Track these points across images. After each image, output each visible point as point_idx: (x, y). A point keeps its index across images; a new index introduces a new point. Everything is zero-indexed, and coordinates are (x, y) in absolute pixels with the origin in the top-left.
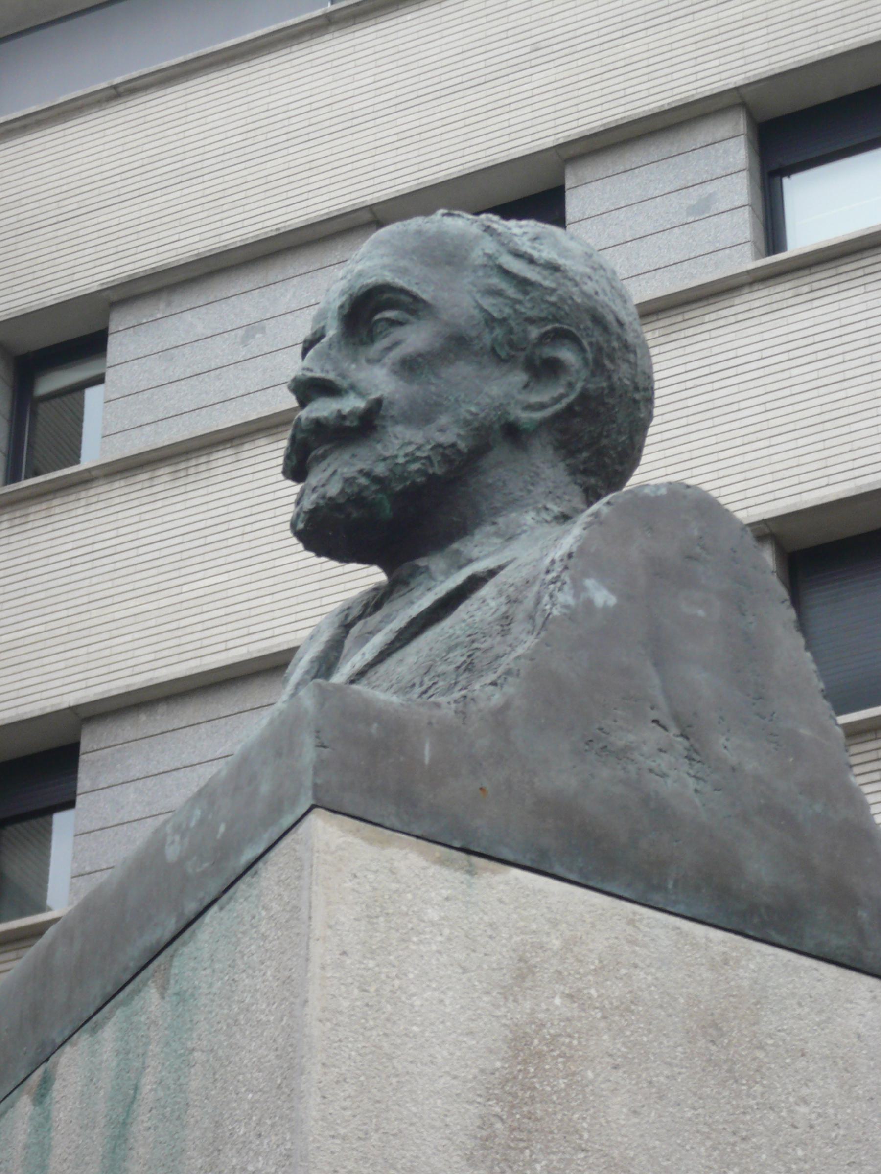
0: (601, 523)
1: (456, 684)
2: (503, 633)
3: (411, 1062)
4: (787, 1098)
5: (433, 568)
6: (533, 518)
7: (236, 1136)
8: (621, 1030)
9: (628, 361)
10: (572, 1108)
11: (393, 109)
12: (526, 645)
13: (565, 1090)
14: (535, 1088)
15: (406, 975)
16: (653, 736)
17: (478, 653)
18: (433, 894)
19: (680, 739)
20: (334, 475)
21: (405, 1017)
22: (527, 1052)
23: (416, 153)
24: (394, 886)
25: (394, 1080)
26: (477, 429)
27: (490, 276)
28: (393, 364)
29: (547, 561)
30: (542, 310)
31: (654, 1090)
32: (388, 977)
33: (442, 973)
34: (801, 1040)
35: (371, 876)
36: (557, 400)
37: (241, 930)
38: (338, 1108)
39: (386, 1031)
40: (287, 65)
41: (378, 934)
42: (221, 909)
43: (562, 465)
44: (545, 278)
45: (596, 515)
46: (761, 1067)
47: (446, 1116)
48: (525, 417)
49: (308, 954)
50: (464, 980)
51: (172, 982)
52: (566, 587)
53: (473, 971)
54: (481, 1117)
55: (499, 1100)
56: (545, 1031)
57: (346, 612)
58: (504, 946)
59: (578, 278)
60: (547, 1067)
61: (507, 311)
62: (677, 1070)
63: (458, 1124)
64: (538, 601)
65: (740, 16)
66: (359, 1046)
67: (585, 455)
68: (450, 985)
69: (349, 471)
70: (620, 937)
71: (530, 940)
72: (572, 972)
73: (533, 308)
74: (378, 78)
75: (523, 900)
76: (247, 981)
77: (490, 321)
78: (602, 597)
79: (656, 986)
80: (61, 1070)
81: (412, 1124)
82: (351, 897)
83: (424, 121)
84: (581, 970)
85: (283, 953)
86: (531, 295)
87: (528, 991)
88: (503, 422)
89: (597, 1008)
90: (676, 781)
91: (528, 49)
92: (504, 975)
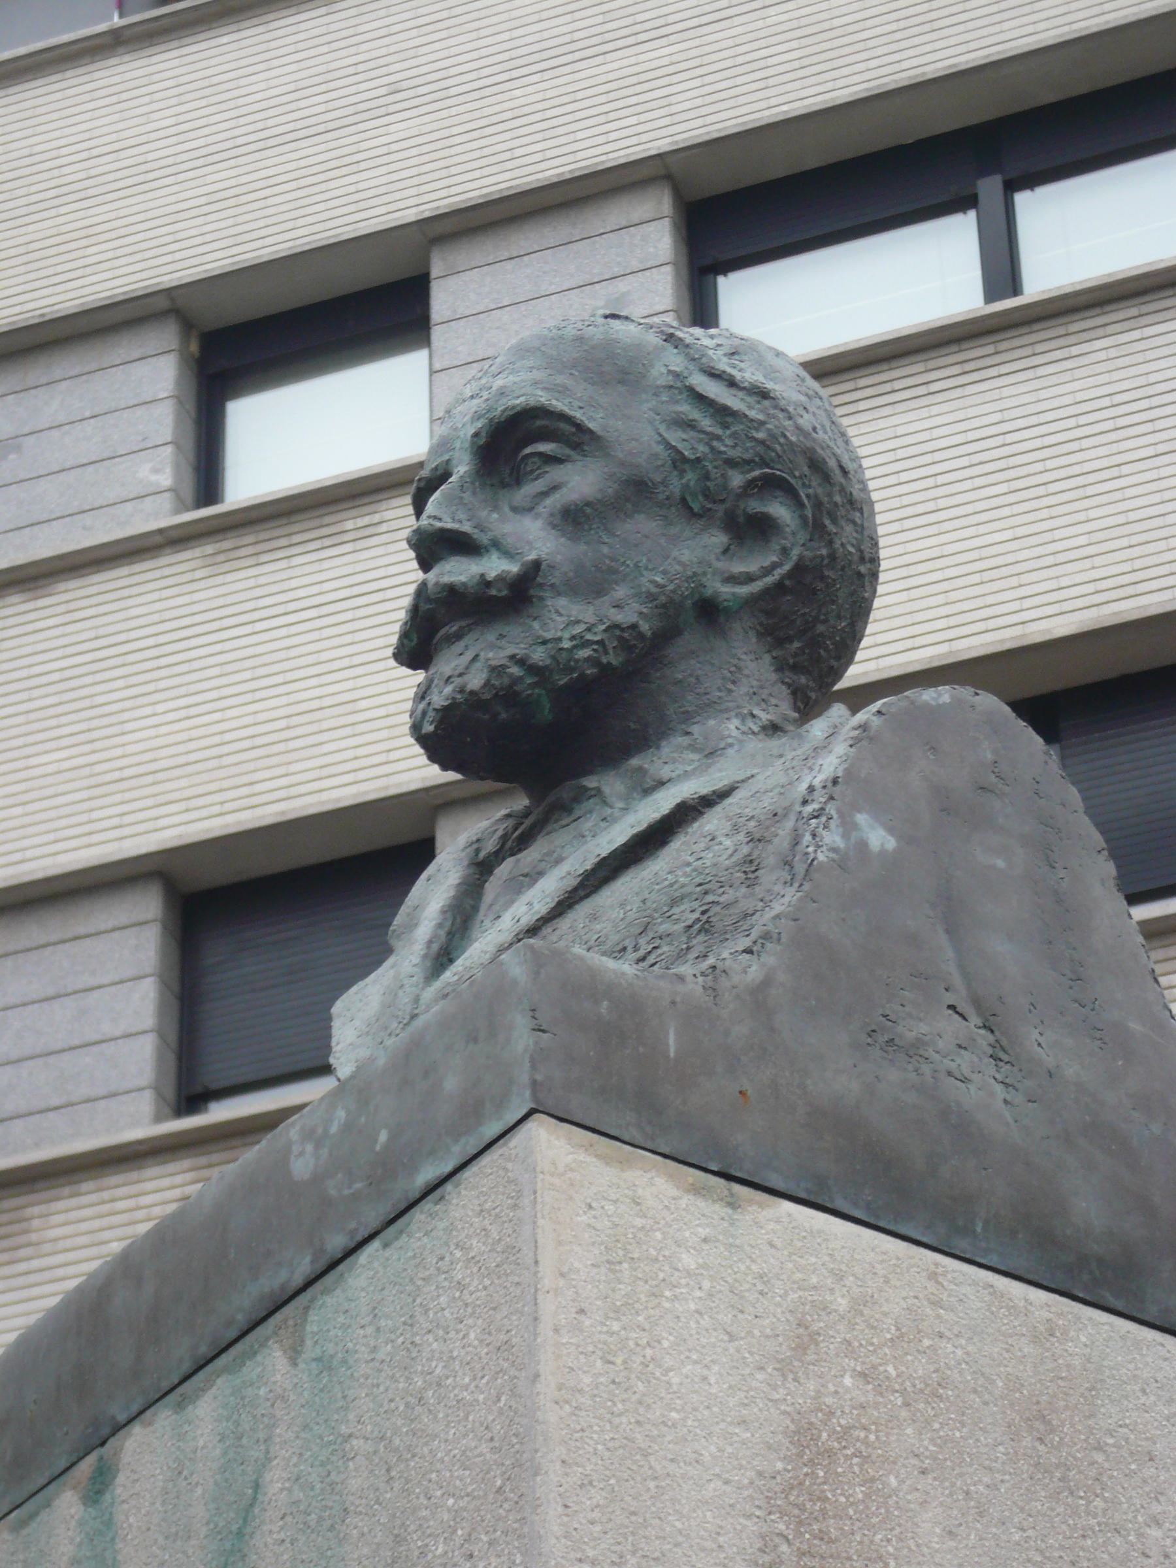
0: (871, 739)
1: (688, 948)
2: (749, 883)
3: (672, 1460)
4: (1135, 1517)
5: (607, 790)
6: (737, 728)
7: (430, 1555)
8: (928, 1422)
9: (854, 522)
10: (874, 1526)
11: (201, 162)
12: (786, 900)
13: (863, 1501)
14: (827, 1498)
15: (659, 1342)
16: (949, 1028)
17: (717, 909)
18: (687, 1234)
19: (983, 1032)
20: (473, 662)
21: (662, 1398)
22: (814, 1449)
23: (231, 222)
24: (639, 1222)
25: (652, 1484)
26: (664, 606)
27: (677, 402)
28: (552, 515)
29: (803, 786)
30: (747, 450)
31: (972, 1503)
32: (637, 1345)
33: (704, 1341)
34: (1147, 1439)
35: (610, 1208)
36: (767, 571)
37: (420, 1275)
38: (584, 1522)
39: (639, 1418)
40: (58, 96)
41: (621, 1286)
42: (386, 1246)
43: (767, 658)
44: (750, 407)
45: (864, 727)
46: (1101, 1474)
47: (718, 1534)
48: (726, 591)
49: (536, 1312)
50: (732, 1351)
51: (309, 1343)
52: (833, 824)
53: (742, 1338)
54: (762, 1537)
55: (783, 1514)
56: (835, 1421)
57: (475, 846)
58: (779, 1305)
59: (791, 409)
60: (840, 1470)
61: (702, 448)
62: (999, 1476)
63: (734, 1545)
64: (796, 842)
65: (665, 61)
66: (607, 1437)
67: (796, 645)
68: (715, 1357)
69: (497, 657)
70: (921, 1296)
71: (810, 1298)
72: (864, 1342)
73: (735, 446)
74: (182, 118)
75: (799, 1244)
76: (435, 1345)
77: (679, 461)
78: (879, 839)
79: (967, 1363)
80: (126, 1457)
81: (677, 1545)
82: (587, 1236)
83: (243, 179)
84: (875, 1340)
85: (494, 1309)
86: (733, 429)
87: (811, 1367)
88: (697, 597)
89: (897, 1391)
90: (982, 1092)
91: (383, 91)
92: (781, 1345)
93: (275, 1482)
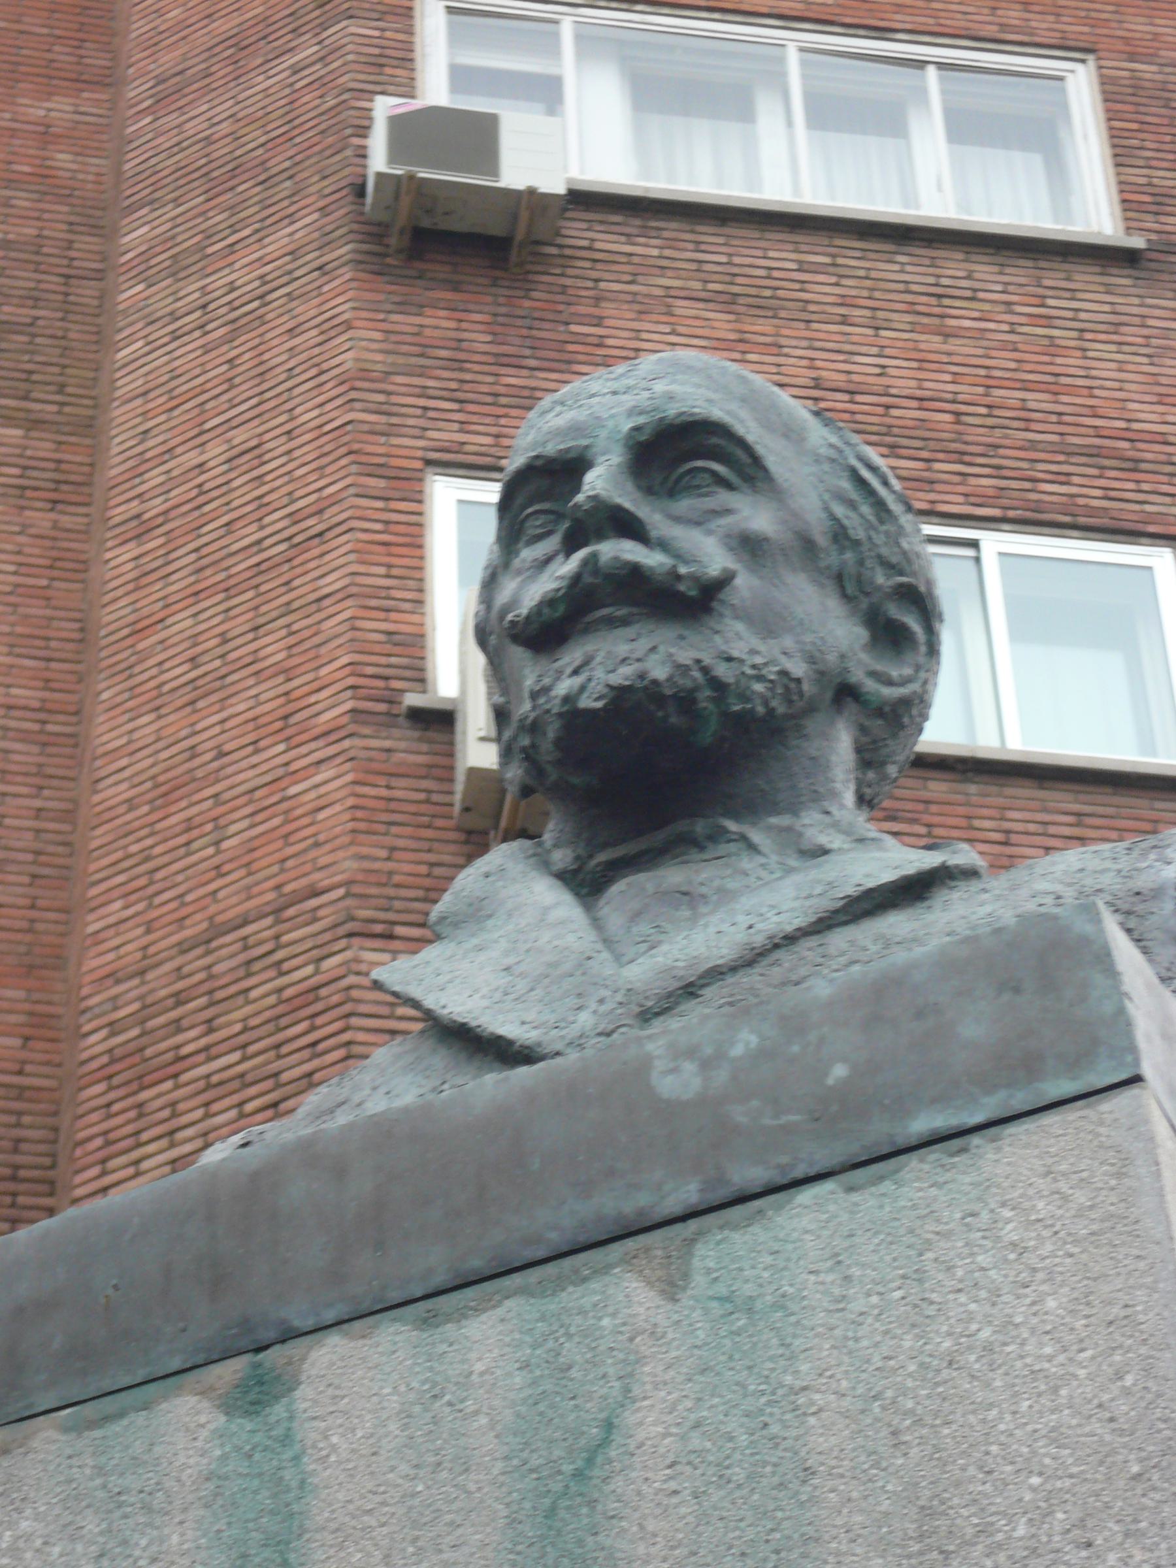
42: (851, 1189)
69: (685, 656)
93: (649, 1424)
